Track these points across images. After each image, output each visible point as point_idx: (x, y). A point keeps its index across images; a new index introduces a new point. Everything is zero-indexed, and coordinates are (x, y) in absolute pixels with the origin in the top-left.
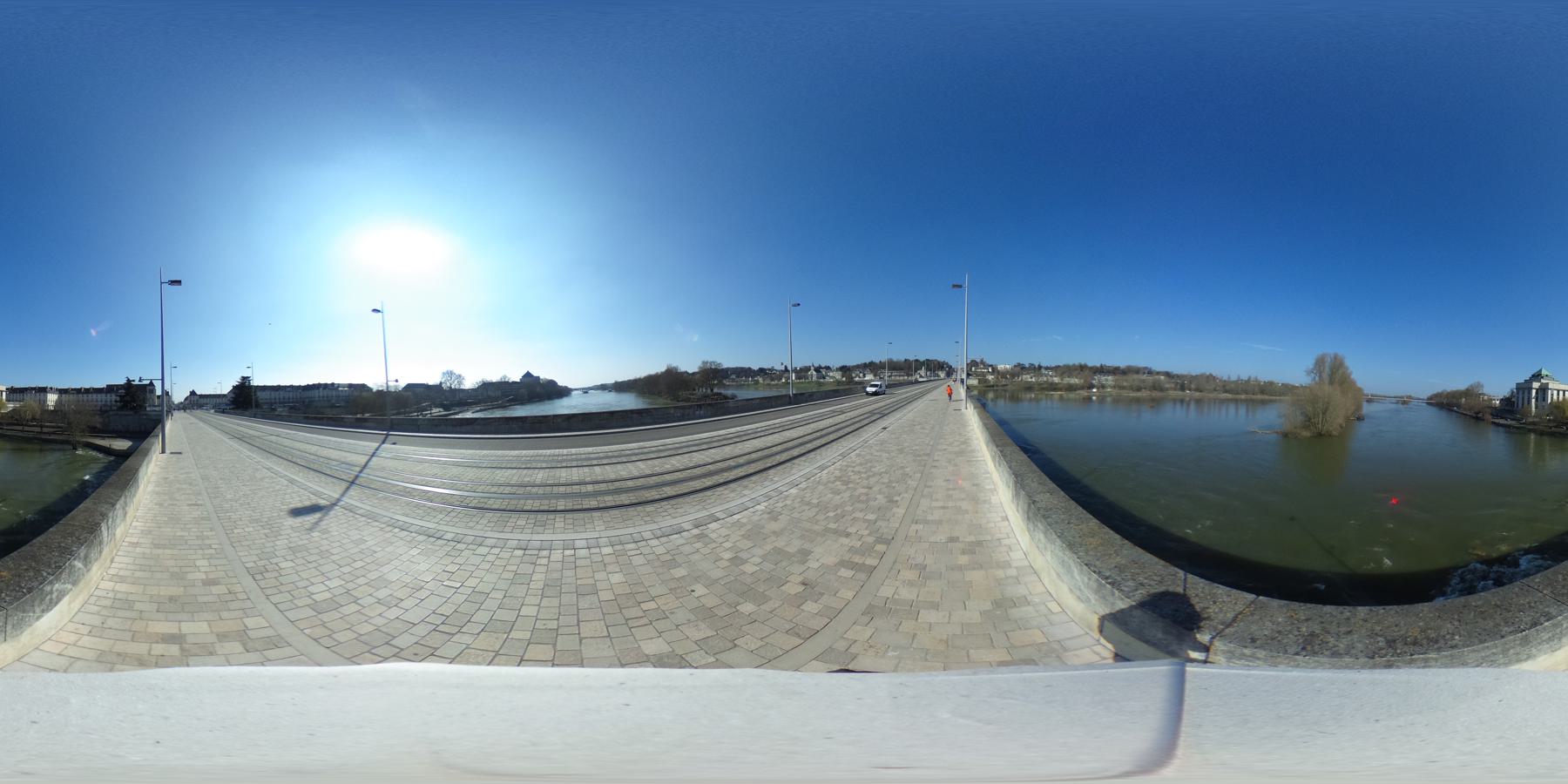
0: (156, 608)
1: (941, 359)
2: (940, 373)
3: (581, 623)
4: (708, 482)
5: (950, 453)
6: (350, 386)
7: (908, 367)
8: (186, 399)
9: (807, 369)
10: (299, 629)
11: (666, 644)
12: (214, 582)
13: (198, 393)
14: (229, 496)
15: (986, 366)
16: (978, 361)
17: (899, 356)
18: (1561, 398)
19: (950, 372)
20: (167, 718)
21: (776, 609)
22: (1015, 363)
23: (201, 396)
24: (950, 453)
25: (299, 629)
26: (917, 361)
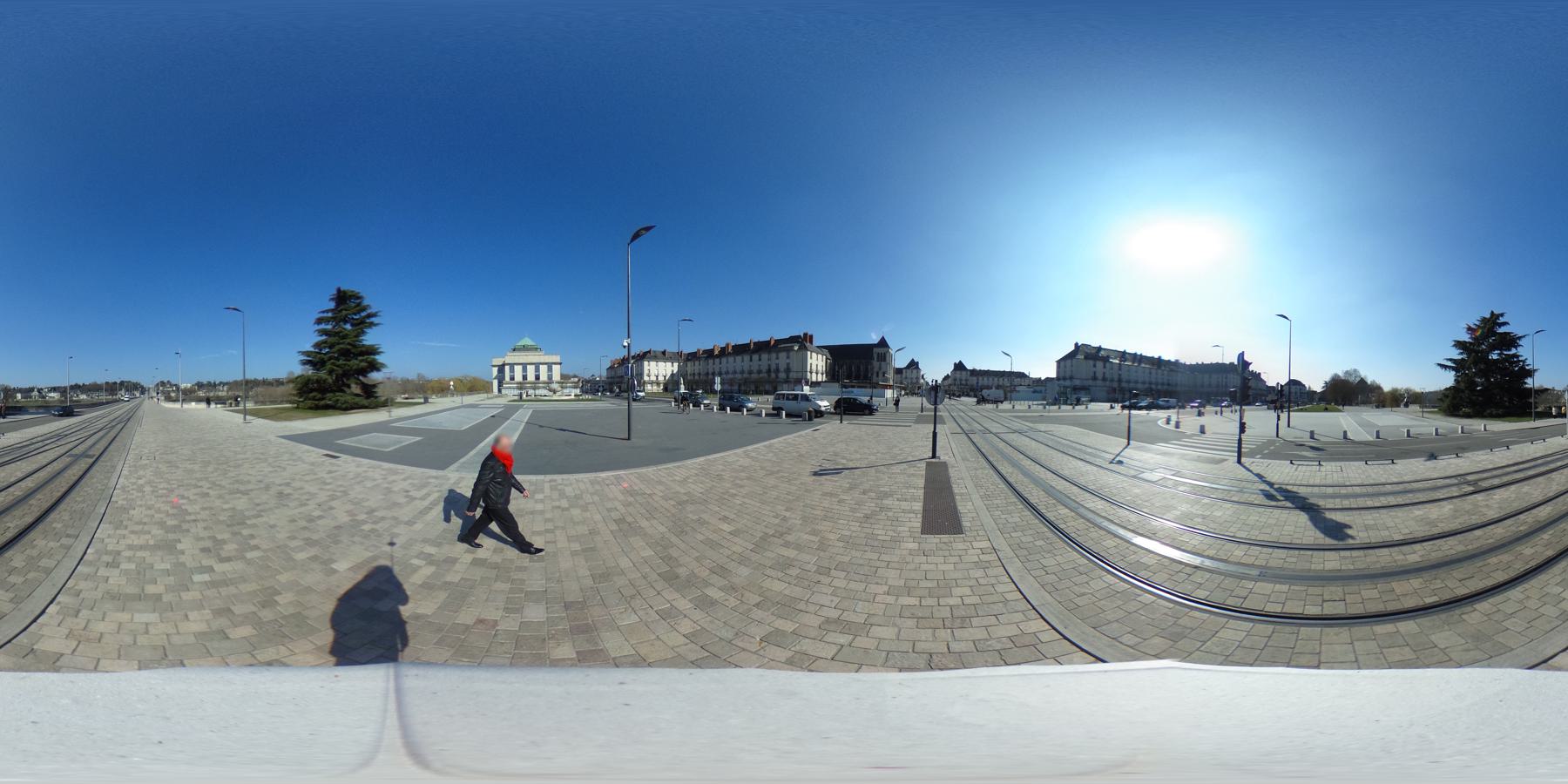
0: (876, 644)
1: (134, 380)
2: (135, 393)
3: (1350, 641)
4: (1400, 500)
5: (383, 469)
6: (1123, 355)
7: (112, 388)
8: (947, 377)
9: (32, 390)
10: (752, 652)
11: (1412, 652)
12: (664, 615)
13: (969, 367)
14: (221, 518)
15: (171, 386)
16: (165, 381)
17: (101, 379)
18: (1284, 416)
19: (143, 390)
20: (168, 719)
21: (1091, 617)
22: (195, 382)
23: (974, 372)
24: (383, 469)
25: (752, 652)
26: (107, 383)
